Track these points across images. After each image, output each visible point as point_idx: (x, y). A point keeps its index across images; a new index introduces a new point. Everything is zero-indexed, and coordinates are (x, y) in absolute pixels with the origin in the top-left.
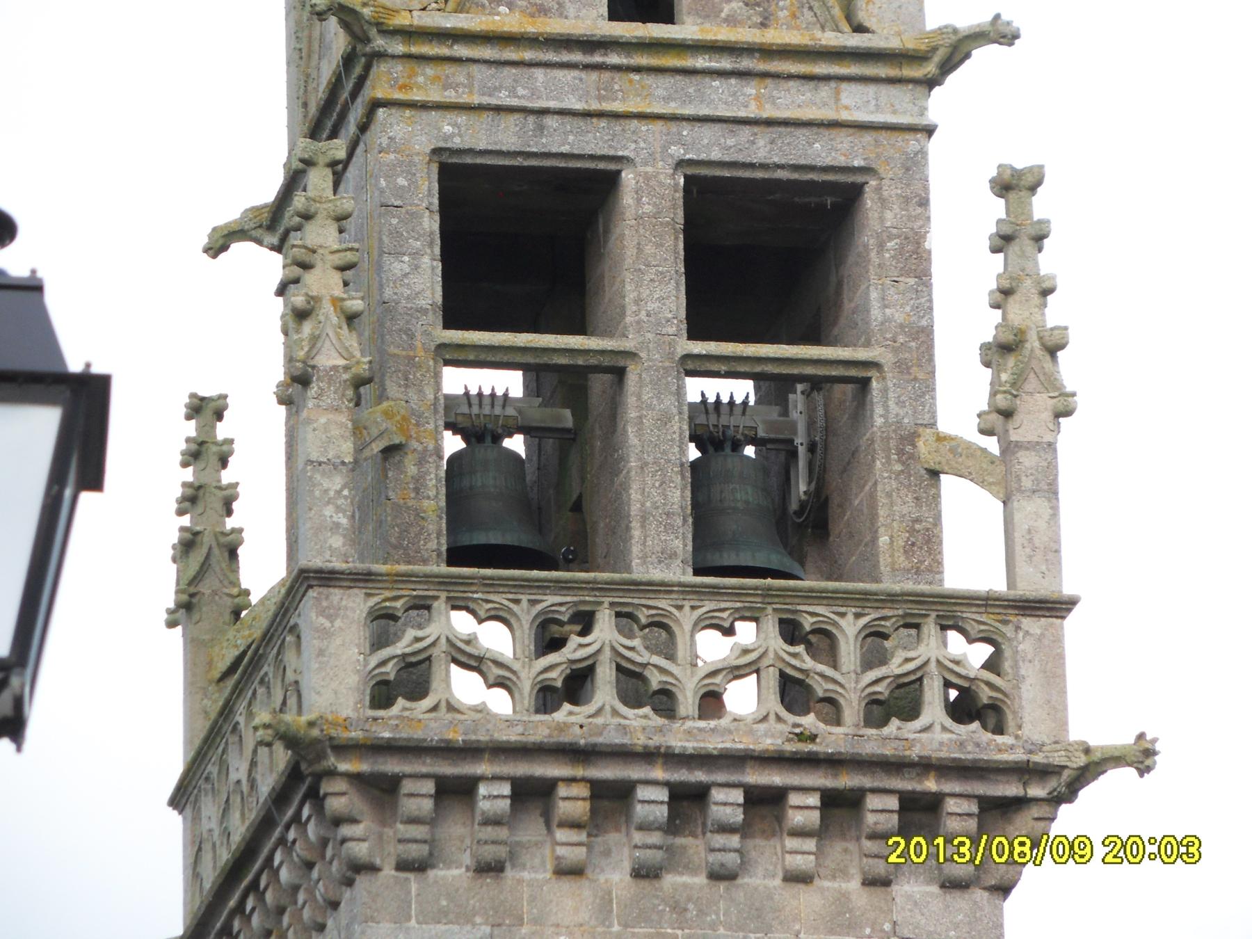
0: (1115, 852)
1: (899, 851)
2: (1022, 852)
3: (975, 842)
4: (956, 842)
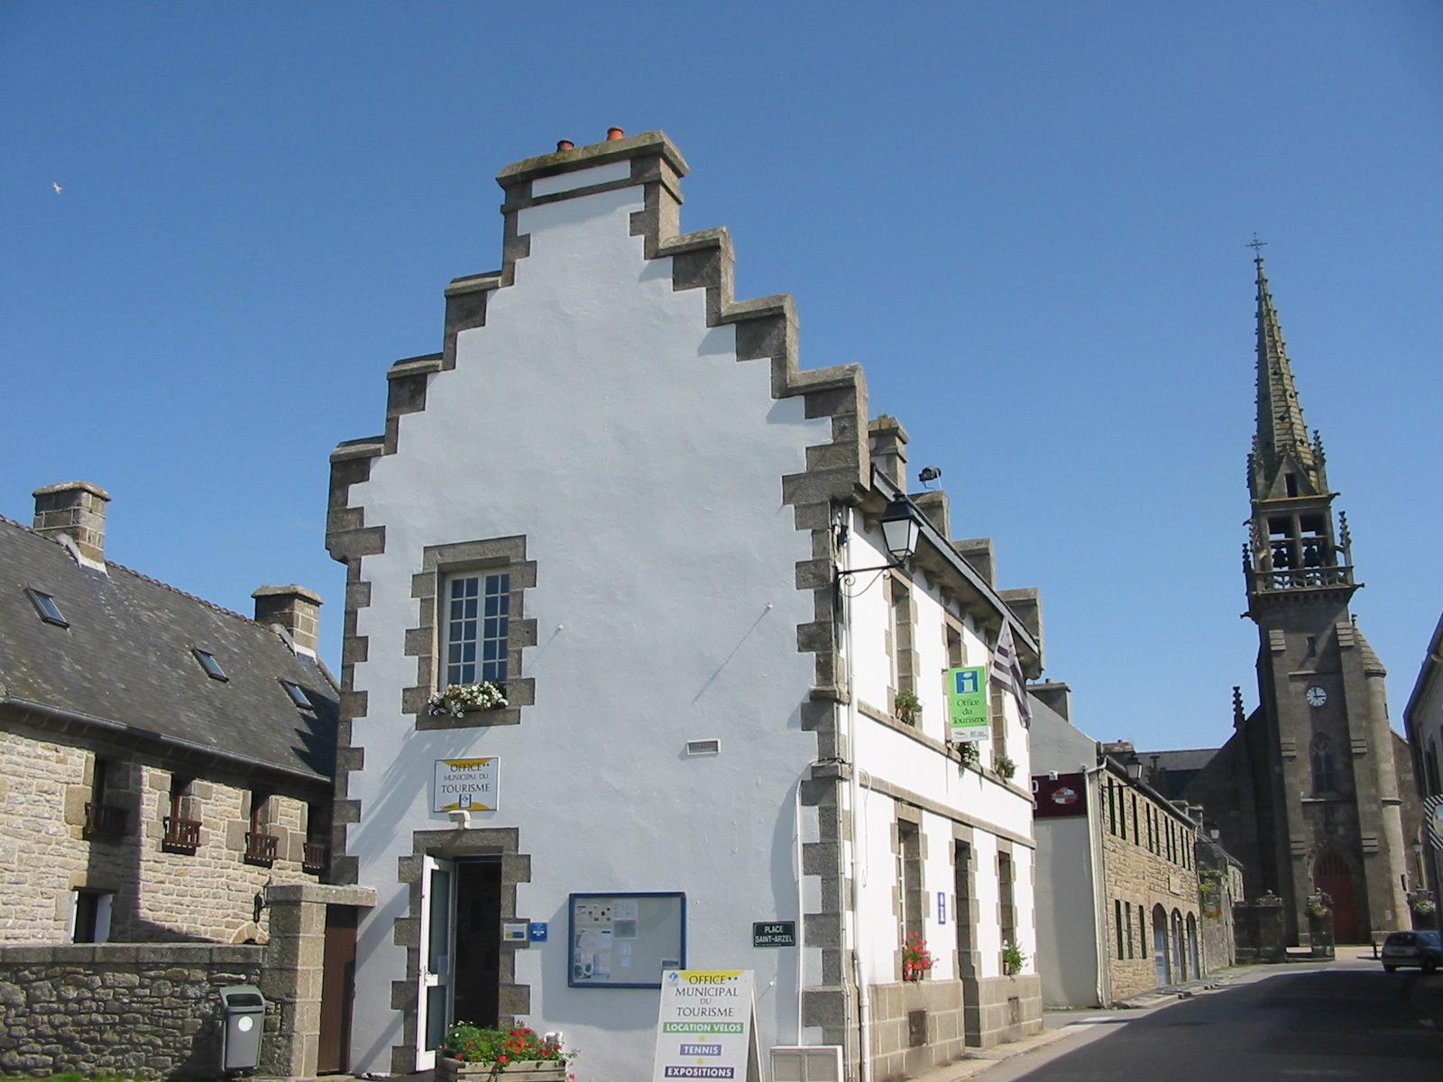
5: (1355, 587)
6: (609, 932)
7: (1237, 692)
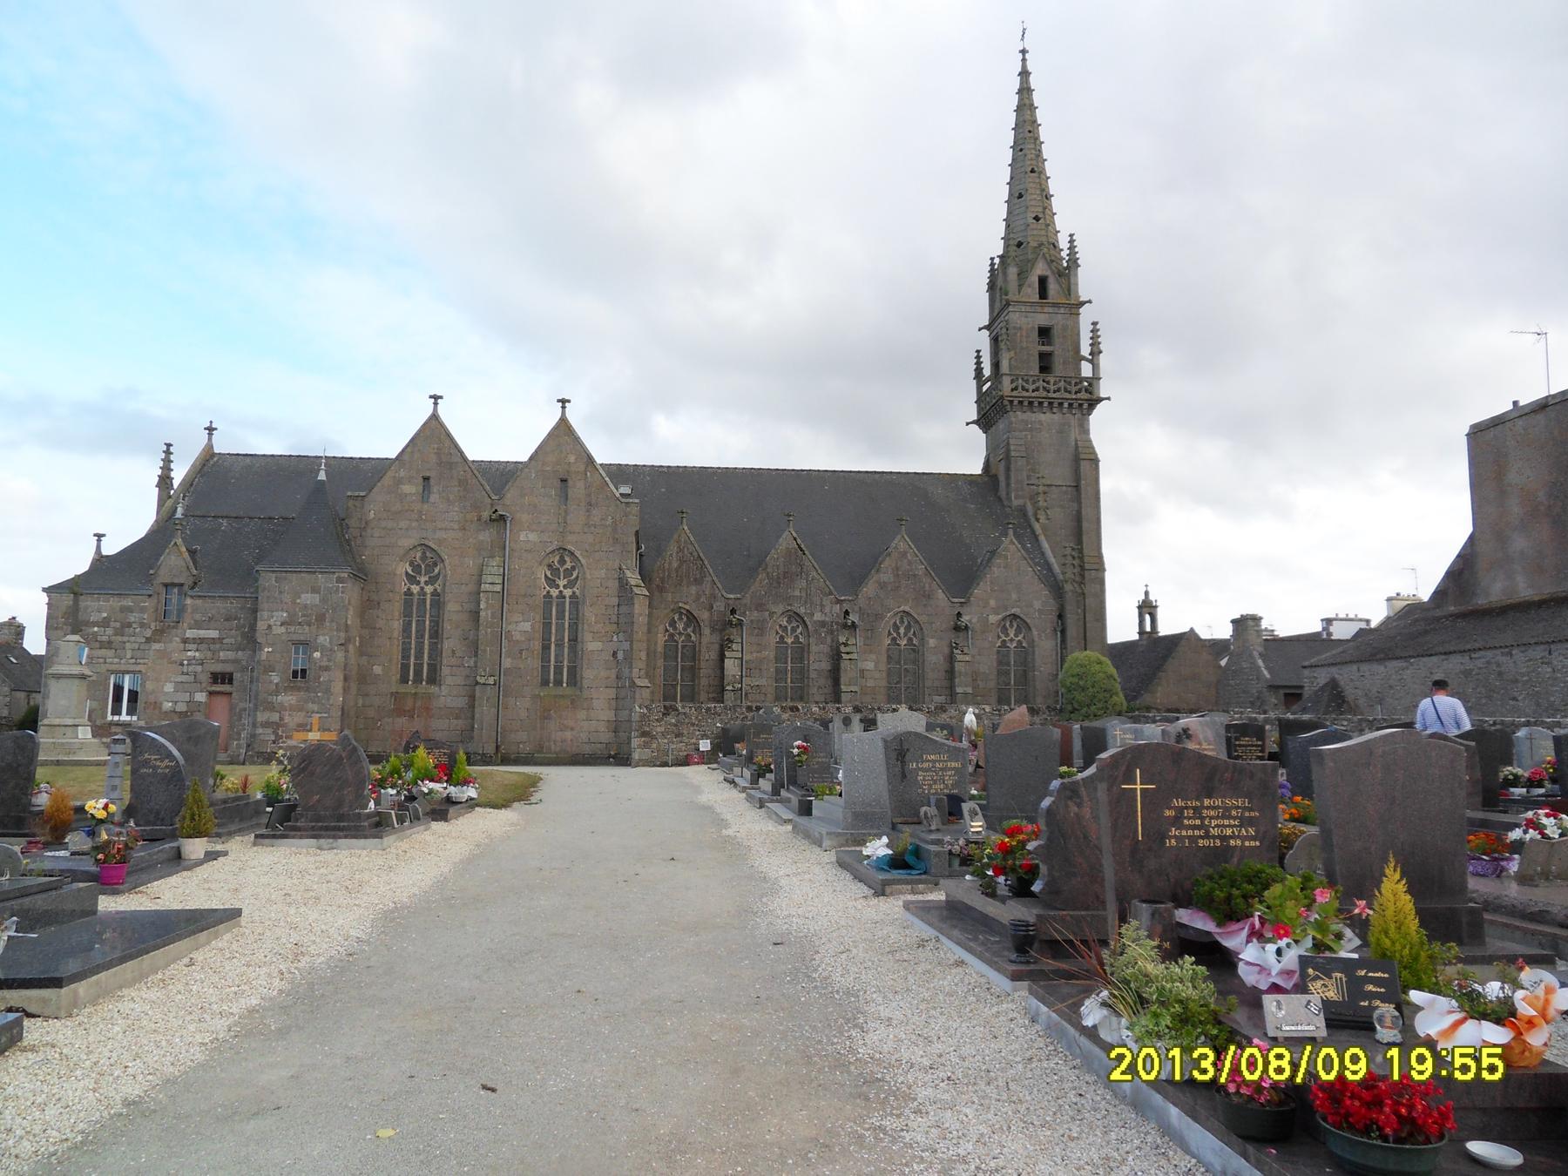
1: (1124, 1065)
2: (1279, 1067)
3: (1220, 1053)
4: (1195, 1055)
5: (1100, 400)
6: (836, 657)
7: (168, 449)
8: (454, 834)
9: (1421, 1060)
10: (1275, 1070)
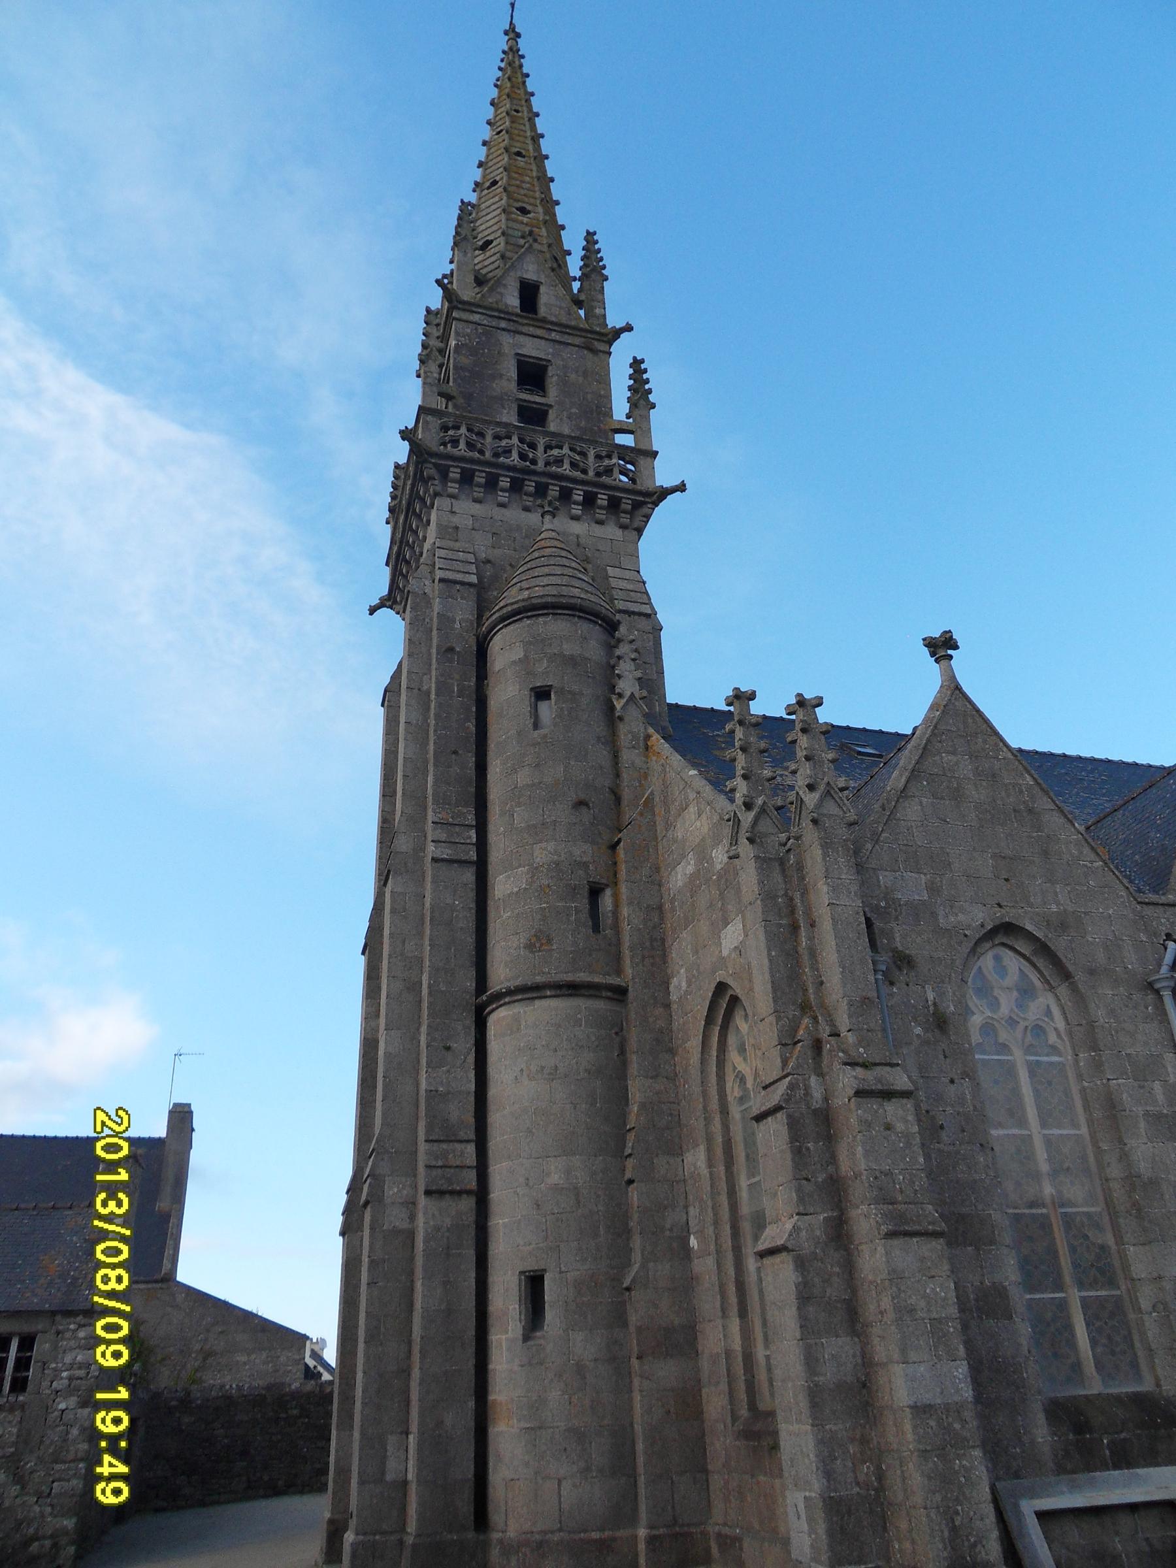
0: (109, 1123)
2: (110, 1279)
4: (121, 1195)
8: (655, 944)
9: (117, 1355)
10: (106, 1275)
